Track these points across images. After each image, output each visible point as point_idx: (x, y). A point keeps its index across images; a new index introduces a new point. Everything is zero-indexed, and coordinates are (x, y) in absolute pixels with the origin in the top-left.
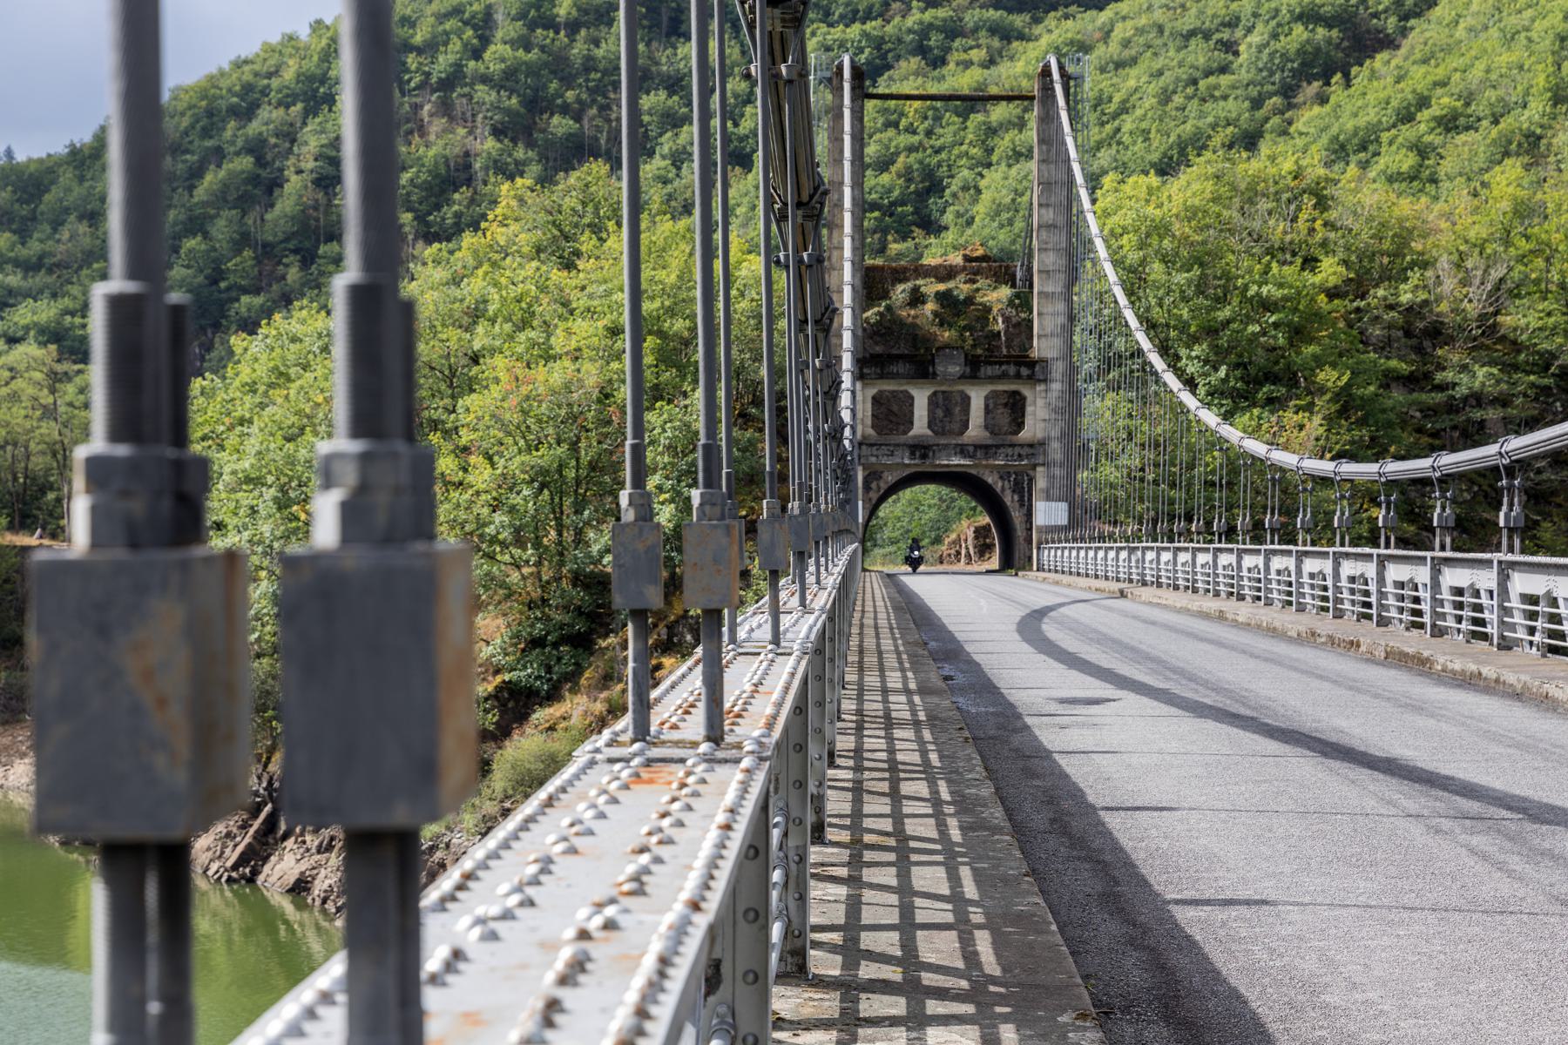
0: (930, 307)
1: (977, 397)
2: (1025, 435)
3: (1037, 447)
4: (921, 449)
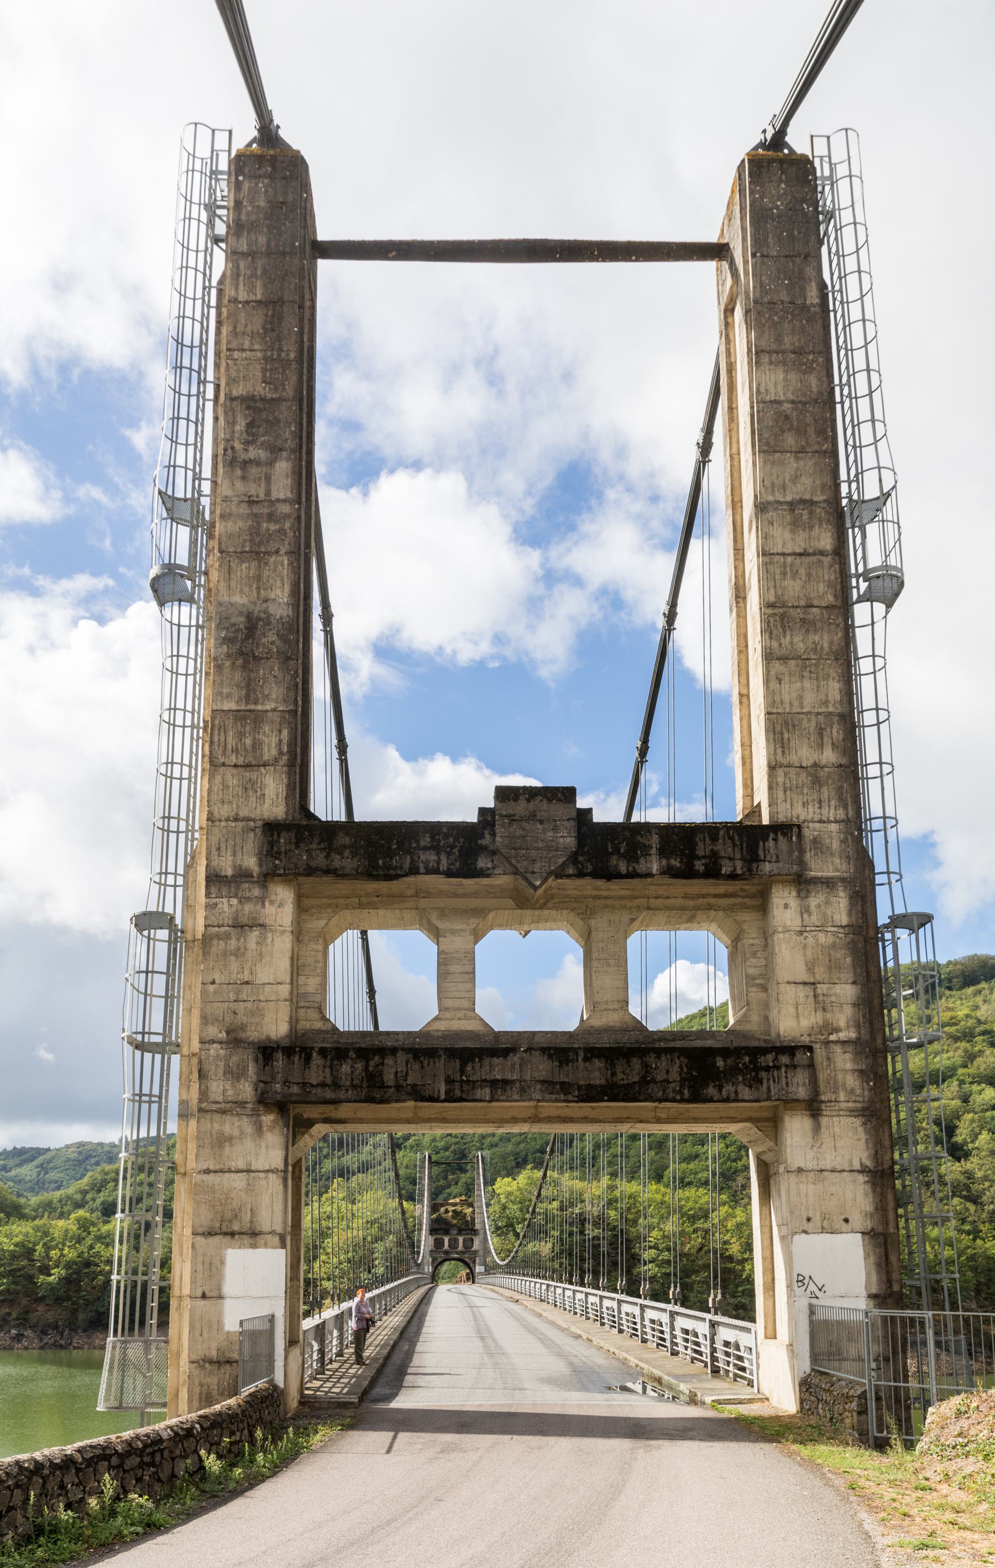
0: (450, 1214)
1: (461, 1239)
2: (473, 1249)
3: (476, 1252)
4: (446, 1253)
